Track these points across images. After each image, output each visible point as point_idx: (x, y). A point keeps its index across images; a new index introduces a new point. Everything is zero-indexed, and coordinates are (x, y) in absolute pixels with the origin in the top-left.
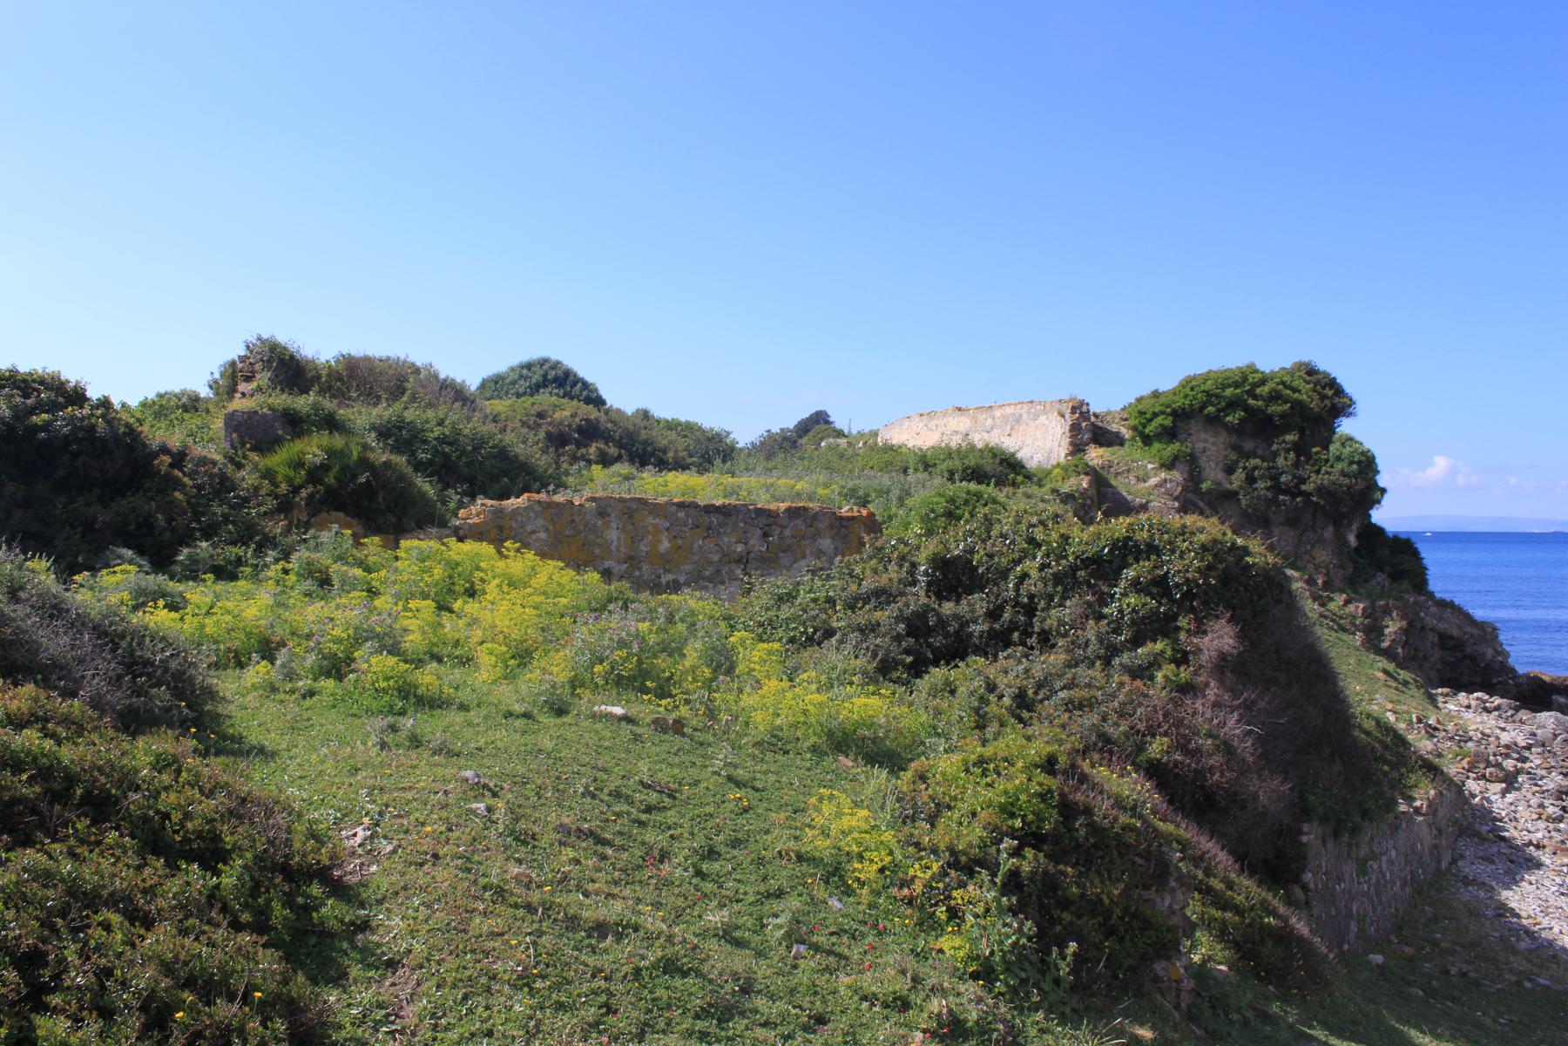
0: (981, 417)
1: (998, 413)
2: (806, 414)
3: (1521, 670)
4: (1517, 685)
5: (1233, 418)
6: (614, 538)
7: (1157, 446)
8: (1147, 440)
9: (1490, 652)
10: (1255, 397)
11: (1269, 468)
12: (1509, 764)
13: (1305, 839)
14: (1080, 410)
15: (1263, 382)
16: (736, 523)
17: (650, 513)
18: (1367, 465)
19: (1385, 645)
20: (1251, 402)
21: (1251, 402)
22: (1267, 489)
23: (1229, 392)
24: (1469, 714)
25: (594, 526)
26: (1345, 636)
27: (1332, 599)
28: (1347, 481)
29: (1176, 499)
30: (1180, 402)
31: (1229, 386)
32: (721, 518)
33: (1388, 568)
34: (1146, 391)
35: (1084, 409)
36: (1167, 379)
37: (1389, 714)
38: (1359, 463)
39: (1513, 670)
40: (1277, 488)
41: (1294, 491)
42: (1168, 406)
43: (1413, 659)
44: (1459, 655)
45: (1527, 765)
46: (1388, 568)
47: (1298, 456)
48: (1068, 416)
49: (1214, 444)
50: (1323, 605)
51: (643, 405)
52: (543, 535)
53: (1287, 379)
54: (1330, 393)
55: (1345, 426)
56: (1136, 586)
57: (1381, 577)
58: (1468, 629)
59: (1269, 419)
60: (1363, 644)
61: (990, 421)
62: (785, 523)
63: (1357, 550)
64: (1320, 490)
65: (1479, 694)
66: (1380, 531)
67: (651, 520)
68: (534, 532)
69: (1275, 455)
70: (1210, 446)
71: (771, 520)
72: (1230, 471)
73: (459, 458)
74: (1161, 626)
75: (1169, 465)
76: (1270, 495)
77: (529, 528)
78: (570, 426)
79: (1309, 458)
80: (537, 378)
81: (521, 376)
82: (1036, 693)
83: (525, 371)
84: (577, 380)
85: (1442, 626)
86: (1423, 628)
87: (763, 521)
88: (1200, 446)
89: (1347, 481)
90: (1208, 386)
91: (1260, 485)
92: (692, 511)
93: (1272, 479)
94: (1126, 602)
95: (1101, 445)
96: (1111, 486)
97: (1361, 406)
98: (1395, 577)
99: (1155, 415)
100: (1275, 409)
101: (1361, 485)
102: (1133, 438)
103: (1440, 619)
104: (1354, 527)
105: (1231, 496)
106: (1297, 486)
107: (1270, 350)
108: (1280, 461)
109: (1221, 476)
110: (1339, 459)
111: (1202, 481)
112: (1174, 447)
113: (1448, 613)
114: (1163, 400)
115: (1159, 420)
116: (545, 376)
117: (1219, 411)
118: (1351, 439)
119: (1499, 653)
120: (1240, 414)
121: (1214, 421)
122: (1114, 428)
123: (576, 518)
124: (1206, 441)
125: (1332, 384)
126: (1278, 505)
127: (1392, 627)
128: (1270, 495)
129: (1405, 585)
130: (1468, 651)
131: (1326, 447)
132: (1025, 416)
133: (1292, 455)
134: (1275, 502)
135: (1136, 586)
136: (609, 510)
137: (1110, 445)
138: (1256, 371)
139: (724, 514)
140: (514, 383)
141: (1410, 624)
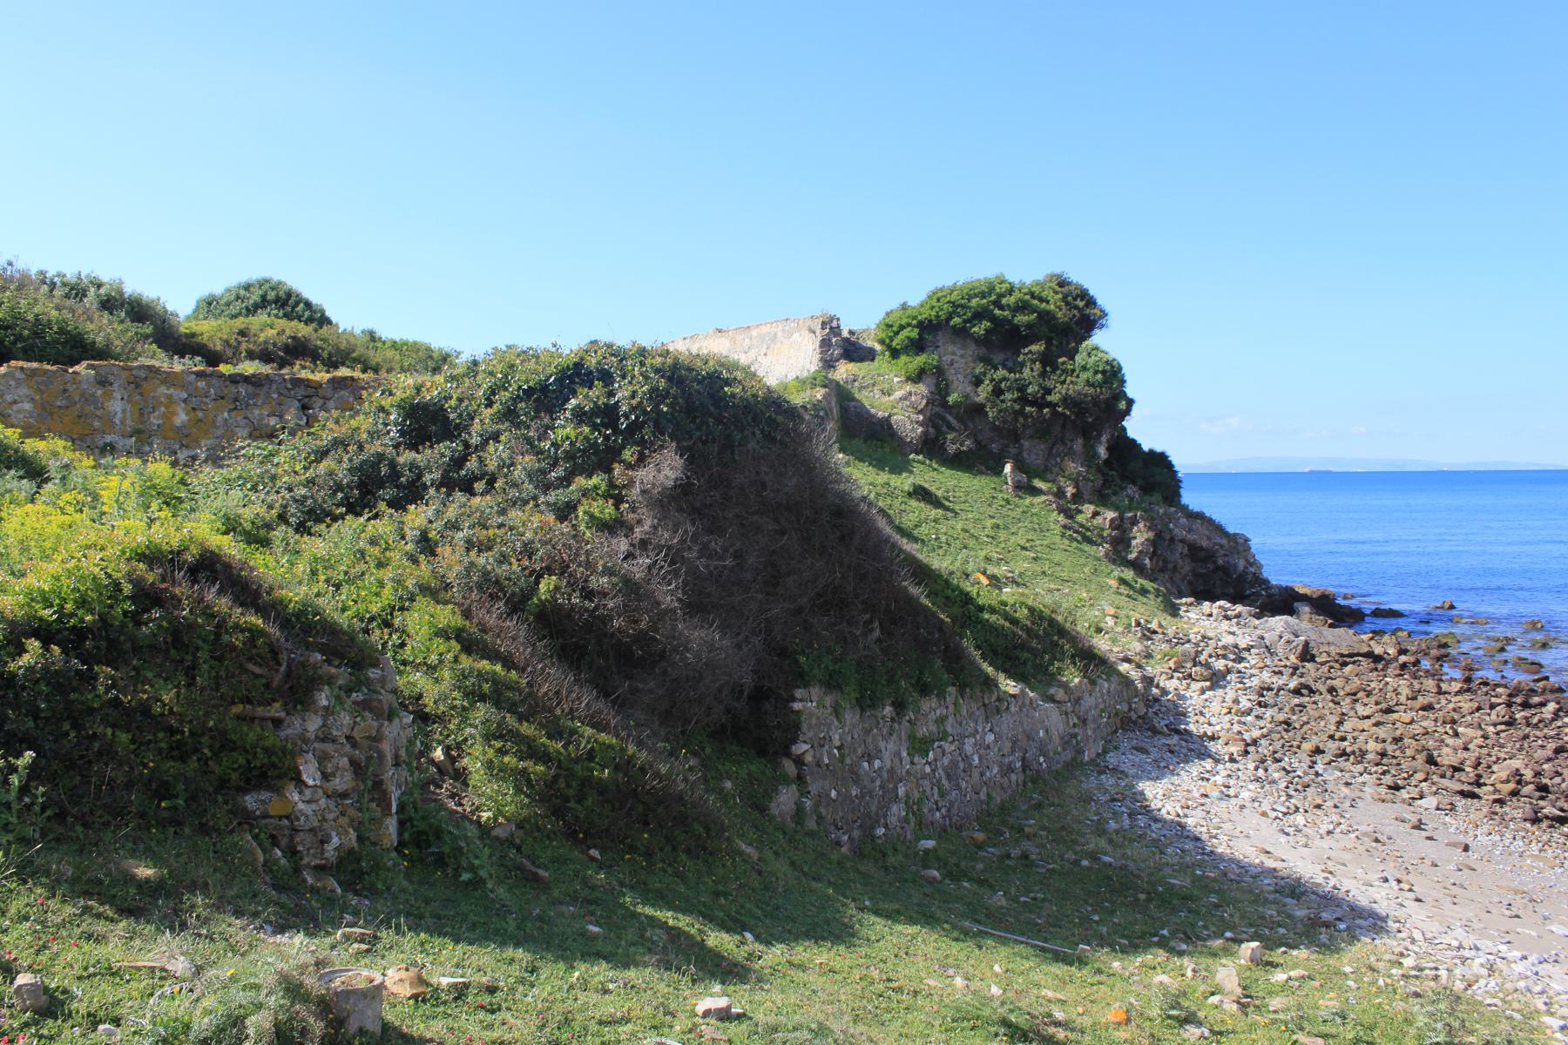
0: (739, 338)
1: (754, 333)
3: (1275, 580)
4: (1269, 596)
5: (980, 329)
6: (118, 409)
7: (903, 358)
9: (1241, 564)
10: (1002, 308)
12: (1219, 665)
13: (797, 706)
14: (830, 326)
15: (1011, 291)
16: (268, 395)
17: (164, 382)
18: (1112, 374)
19: (1132, 556)
20: (997, 312)
21: (997, 312)
22: (1014, 401)
23: (974, 302)
24: (1208, 622)
25: (93, 395)
26: (1086, 547)
27: (1081, 512)
28: (1091, 391)
29: (920, 412)
30: (927, 314)
32: (250, 388)
33: (1140, 482)
34: (894, 304)
35: (834, 324)
36: (916, 296)
37: (1108, 619)
38: (1104, 372)
39: (1266, 581)
40: (1024, 400)
41: (1040, 403)
42: (915, 318)
43: (1162, 570)
44: (1211, 566)
45: (1240, 666)
46: (1140, 482)
47: (1044, 367)
48: (818, 332)
49: (962, 356)
50: (1071, 517)
51: (369, 326)
52: (27, 406)
53: (1036, 290)
54: (1081, 304)
55: (1098, 338)
56: (580, 416)
57: (1132, 490)
58: (1218, 540)
59: (1016, 328)
60: (1106, 555)
62: (329, 394)
63: (1106, 461)
64: (1066, 400)
65: (1222, 603)
66: (1134, 444)
67: (163, 390)
68: (15, 402)
69: (1022, 365)
70: (958, 359)
71: (310, 391)
72: (978, 382)
73: (14, 343)
74: (599, 459)
75: (917, 377)
76: (1017, 407)
77: (9, 398)
78: (274, 344)
79: (1055, 368)
80: (255, 298)
81: (238, 297)
83: (242, 292)
84: (299, 299)
85: (1190, 537)
86: (1172, 539)
87: (301, 392)
88: (947, 358)
89: (1091, 391)
90: (954, 297)
91: (1008, 396)
92: (214, 381)
94: (565, 430)
95: (851, 360)
96: (854, 399)
97: (1112, 320)
98: (1147, 489)
99: (902, 327)
100: (1021, 319)
101: (1106, 394)
102: (883, 354)
103: (1190, 530)
104: (1104, 438)
105: (979, 409)
106: (1043, 397)
107: (1024, 265)
108: (1027, 372)
109: (969, 389)
110: (1084, 368)
111: (948, 394)
112: (920, 360)
113: (1198, 524)
114: (909, 312)
116: (264, 297)
117: (965, 321)
119: (1251, 565)
120: (986, 324)
121: (961, 333)
122: (869, 343)
123: (69, 386)
125: (1084, 294)
126: (1026, 416)
127: (1140, 537)
128: (1017, 407)
129: (1157, 497)
130: (1220, 562)
131: (1072, 358)
134: (1021, 412)
135: (580, 416)
136: (111, 379)
137: (861, 360)
138: (1003, 282)
139: (253, 384)
140: (228, 304)
141: (1159, 535)
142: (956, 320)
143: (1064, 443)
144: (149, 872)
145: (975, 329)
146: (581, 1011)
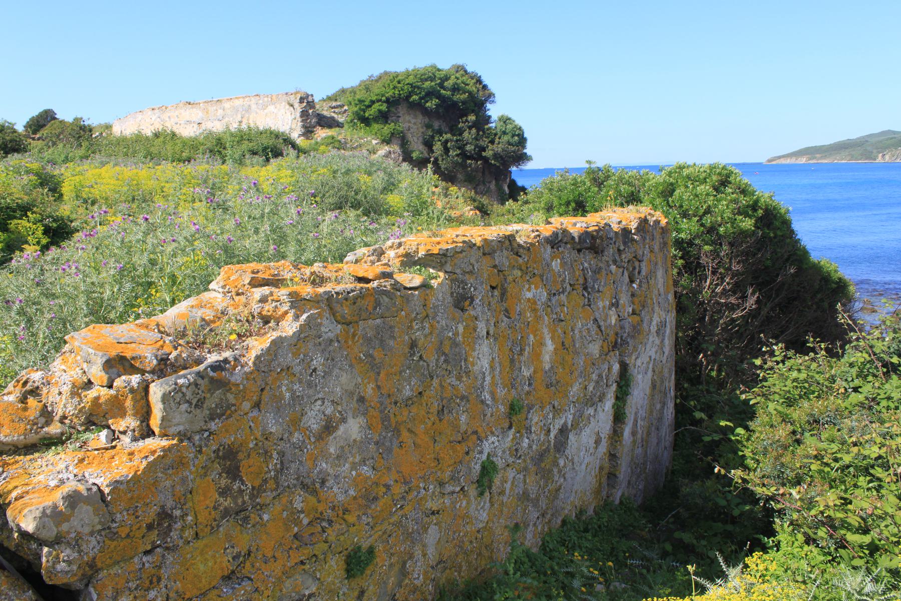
0: (212, 109)
2: (35, 112)
5: (431, 104)
8: (366, 121)
11: (457, 141)
14: (307, 101)
20: (443, 92)
21: (443, 92)
22: (457, 155)
23: (427, 84)
31: (426, 80)
35: (310, 99)
40: (464, 155)
48: (297, 105)
49: (415, 124)
59: (455, 104)
61: (220, 112)
64: (496, 156)
68: (329, 428)
70: (412, 124)
75: (387, 141)
76: (460, 160)
77: (313, 420)
82: (286, 313)
90: (411, 79)
93: (459, 148)
95: (323, 126)
97: (498, 98)
99: (373, 102)
108: (466, 135)
115: (376, 106)
117: (421, 98)
118: (509, 119)
120: (435, 101)
121: (418, 107)
124: (409, 122)
132: (254, 107)
133: (474, 131)
137: (330, 127)
138: (439, 70)
142: (415, 97)
143: (484, 184)
144: (485, 363)
145: (428, 104)
146: (465, 536)
